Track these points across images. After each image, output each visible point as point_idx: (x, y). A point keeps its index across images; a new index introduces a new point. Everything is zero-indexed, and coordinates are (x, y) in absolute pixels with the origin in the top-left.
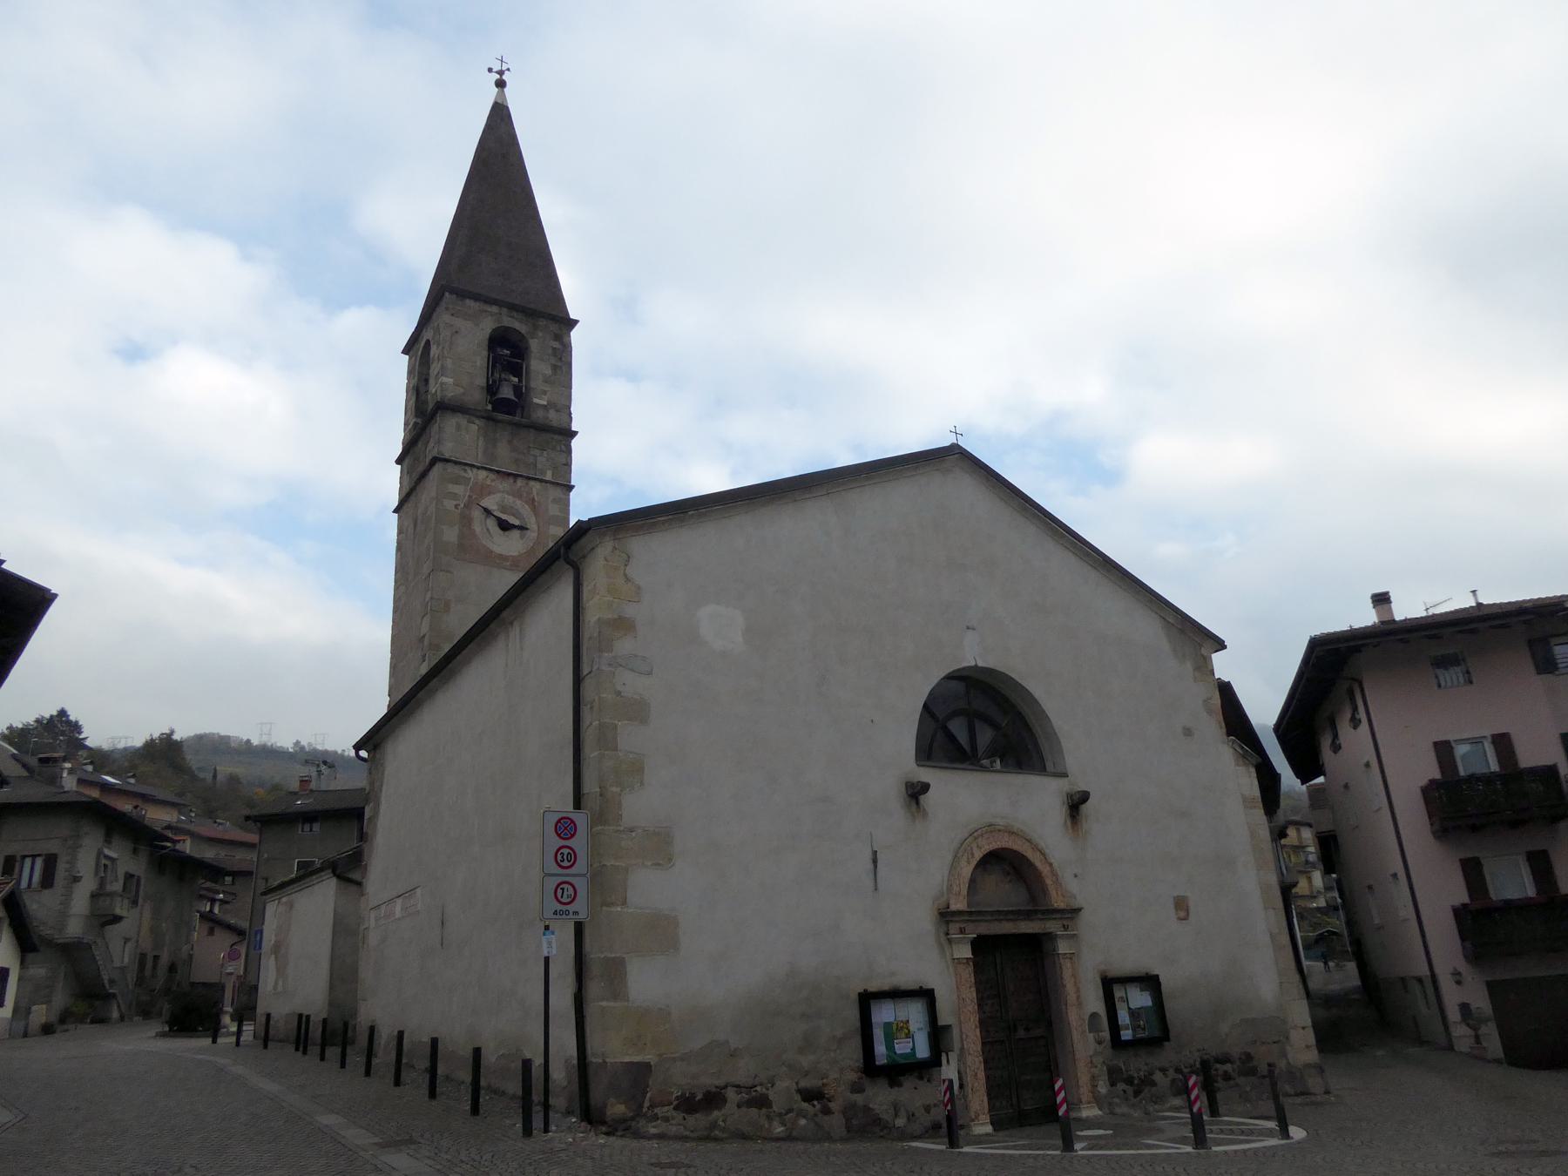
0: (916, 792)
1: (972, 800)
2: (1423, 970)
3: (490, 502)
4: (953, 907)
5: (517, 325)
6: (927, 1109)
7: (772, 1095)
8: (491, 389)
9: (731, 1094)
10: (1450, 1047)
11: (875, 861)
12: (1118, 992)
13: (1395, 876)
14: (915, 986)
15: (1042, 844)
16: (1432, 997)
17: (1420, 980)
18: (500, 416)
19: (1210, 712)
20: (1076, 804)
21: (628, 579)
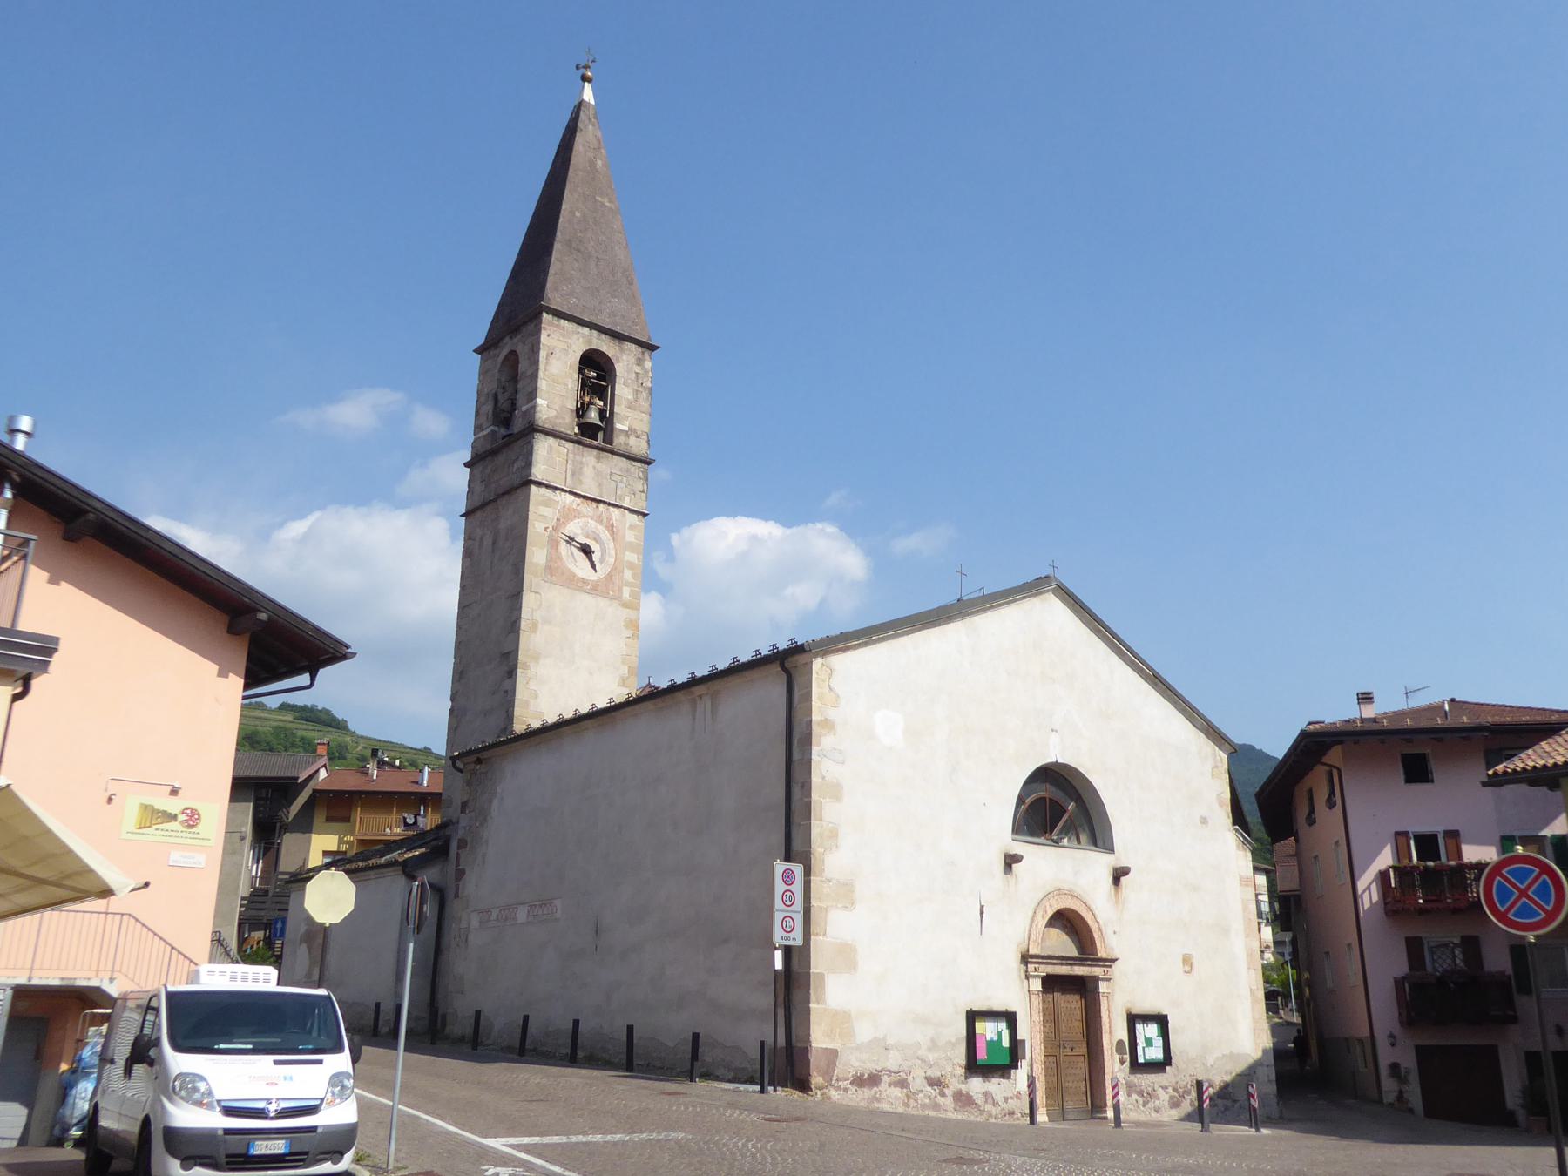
0: (1011, 861)
1: (1060, 869)
2: (1365, 1033)
3: (573, 528)
4: (1032, 952)
5: (604, 349)
6: (1006, 1099)
7: (910, 1079)
8: (581, 412)
9: (886, 1079)
10: (1380, 1101)
11: (982, 913)
12: (1139, 1028)
13: (1349, 945)
14: (1002, 1009)
15: (1093, 907)
16: (1370, 1059)
17: (1361, 1041)
18: (585, 440)
19: (1221, 805)
20: (1119, 875)
21: (831, 689)
